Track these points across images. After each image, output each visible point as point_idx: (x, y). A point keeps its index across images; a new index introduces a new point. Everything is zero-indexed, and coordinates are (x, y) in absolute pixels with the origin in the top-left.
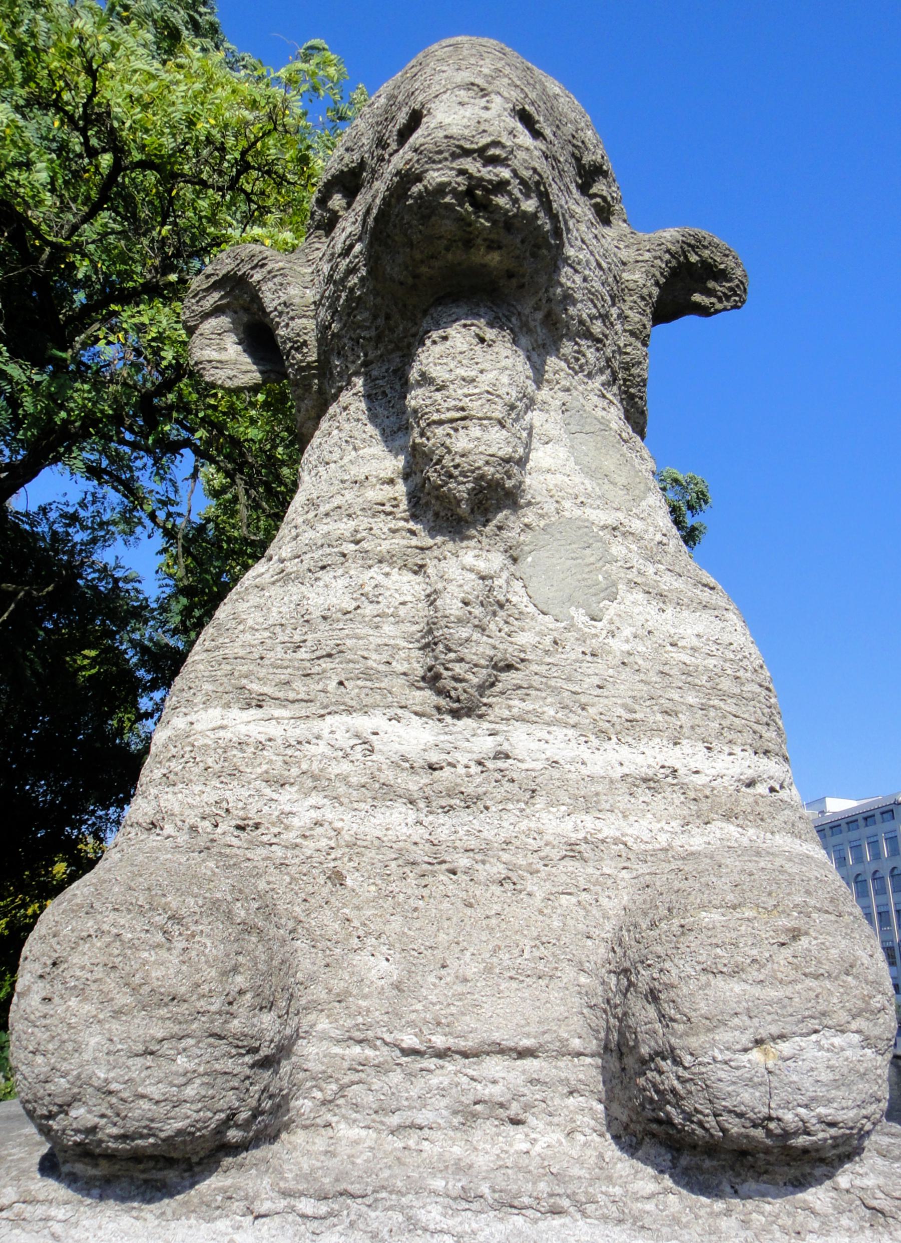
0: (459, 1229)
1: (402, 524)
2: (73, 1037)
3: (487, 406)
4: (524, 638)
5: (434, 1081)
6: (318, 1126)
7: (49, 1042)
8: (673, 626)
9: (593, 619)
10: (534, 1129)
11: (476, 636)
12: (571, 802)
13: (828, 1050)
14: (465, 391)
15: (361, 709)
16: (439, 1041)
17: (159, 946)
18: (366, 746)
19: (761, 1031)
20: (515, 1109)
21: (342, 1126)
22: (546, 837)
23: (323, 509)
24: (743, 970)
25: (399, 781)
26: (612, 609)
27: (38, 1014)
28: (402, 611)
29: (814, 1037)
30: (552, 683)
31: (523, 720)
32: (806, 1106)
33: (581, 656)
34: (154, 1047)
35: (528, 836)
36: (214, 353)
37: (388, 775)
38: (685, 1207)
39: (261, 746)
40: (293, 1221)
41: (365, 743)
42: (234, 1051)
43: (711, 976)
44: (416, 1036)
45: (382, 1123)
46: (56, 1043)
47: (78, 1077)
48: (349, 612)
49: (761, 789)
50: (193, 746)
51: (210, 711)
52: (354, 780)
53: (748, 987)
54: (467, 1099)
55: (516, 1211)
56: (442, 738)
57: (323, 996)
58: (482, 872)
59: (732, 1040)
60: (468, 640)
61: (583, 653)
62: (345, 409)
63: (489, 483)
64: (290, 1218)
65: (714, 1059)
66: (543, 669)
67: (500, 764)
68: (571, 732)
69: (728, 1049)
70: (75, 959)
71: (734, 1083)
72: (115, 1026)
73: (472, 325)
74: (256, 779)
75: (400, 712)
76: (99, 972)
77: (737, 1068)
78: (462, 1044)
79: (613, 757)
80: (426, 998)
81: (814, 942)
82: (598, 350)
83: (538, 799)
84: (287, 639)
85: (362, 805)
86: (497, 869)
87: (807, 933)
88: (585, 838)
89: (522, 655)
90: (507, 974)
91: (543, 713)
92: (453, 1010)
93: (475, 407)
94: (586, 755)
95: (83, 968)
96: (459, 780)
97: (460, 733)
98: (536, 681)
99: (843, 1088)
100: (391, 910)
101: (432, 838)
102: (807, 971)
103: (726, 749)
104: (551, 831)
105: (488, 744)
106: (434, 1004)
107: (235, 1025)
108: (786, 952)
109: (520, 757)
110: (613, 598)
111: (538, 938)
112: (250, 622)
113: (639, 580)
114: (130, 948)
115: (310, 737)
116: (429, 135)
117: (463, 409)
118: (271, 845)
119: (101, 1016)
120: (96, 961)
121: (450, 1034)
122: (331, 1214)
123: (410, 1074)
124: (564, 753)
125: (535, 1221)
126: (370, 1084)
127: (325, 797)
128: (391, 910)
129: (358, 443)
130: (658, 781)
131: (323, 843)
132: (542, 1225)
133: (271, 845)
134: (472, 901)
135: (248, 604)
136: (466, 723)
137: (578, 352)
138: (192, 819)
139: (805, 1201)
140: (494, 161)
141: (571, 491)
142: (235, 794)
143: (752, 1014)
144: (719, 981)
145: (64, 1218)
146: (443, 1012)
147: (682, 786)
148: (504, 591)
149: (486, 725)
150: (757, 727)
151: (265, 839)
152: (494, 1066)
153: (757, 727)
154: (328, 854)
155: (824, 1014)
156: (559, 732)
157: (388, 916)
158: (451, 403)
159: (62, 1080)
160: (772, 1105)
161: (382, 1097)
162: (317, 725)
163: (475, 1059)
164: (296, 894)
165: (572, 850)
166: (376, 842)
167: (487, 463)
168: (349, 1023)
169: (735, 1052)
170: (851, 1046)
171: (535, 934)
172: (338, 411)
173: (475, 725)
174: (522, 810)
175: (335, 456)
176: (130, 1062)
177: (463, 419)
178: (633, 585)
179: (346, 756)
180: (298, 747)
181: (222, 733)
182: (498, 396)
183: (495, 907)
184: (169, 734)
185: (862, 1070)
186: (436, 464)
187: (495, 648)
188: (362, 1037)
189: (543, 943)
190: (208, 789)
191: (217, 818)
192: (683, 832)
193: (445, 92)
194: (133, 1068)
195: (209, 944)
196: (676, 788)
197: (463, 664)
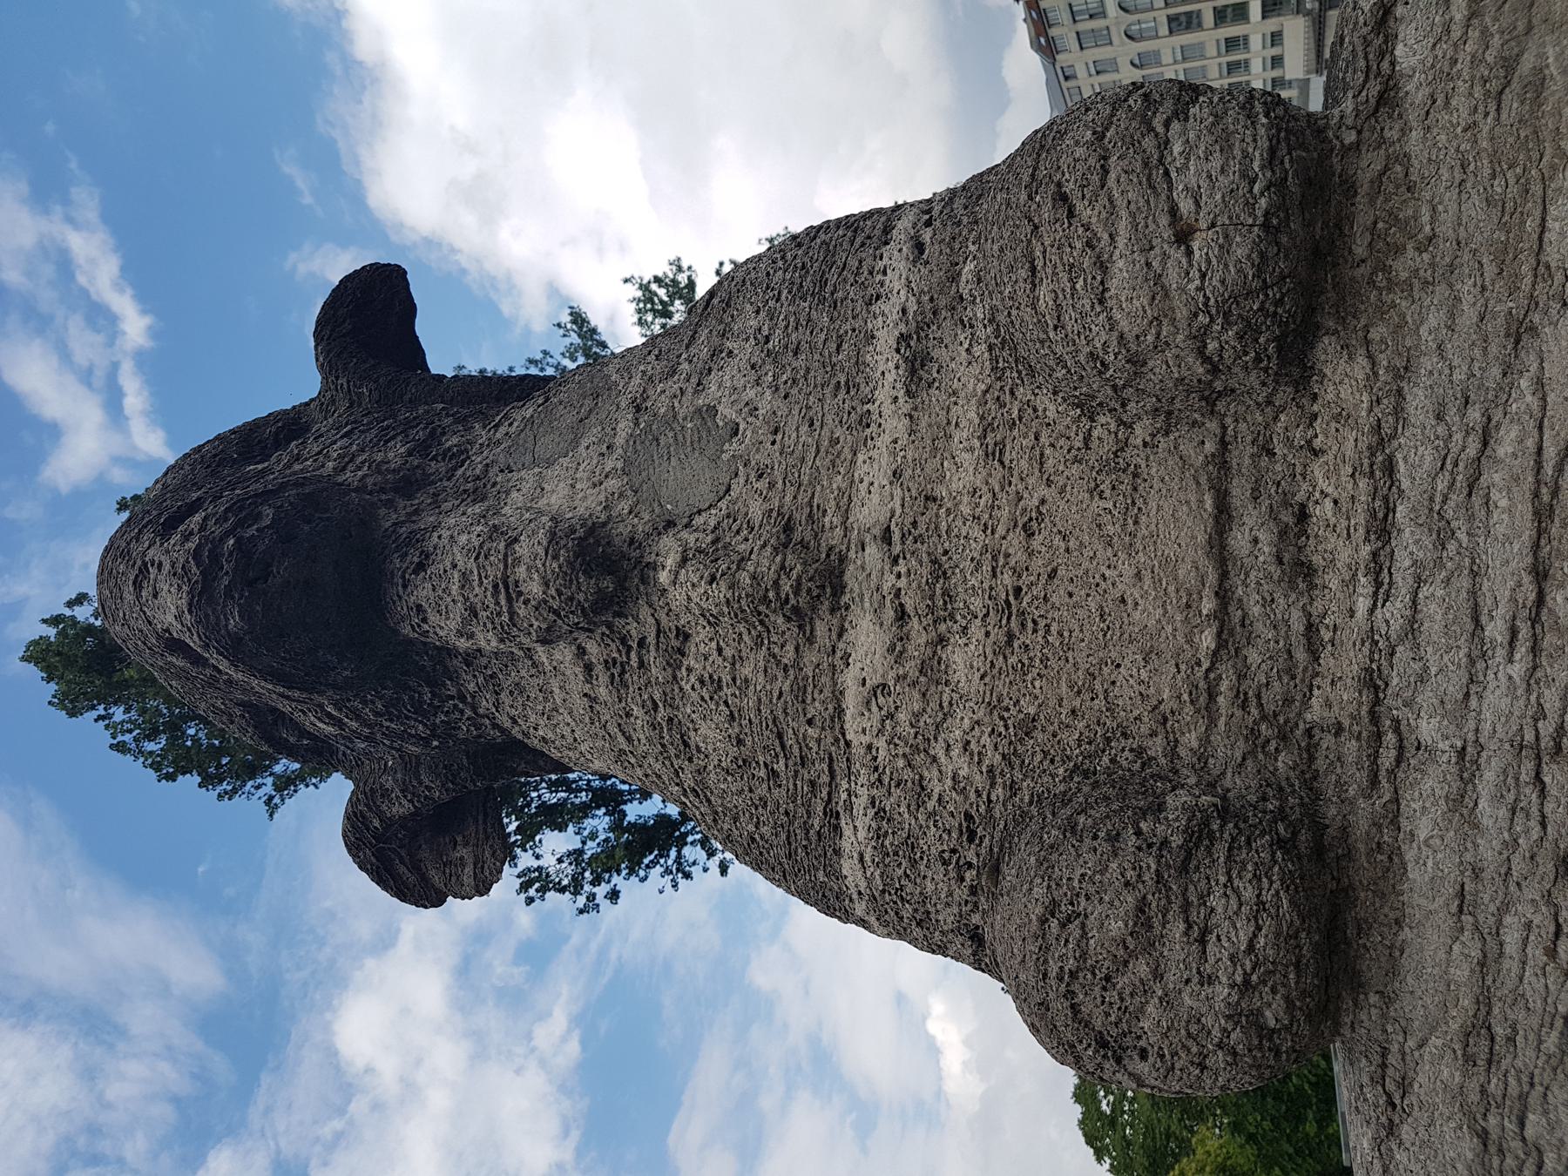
0: (1410, 580)
1: (633, 655)
2: (1183, 1024)
3: (492, 558)
4: (756, 510)
5: (1256, 610)
6: (1309, 744)
7: (1189, 1050)
8: (747, 340)
9: (736, 434)
10: (1311, 494)
11: (750, 567)
12: (939, 456)
13: (1188, 159)
14: (476, 583)
15: (839, 701)
16: (1208, 605)
17: (1083, 926)
18: (879, 692)
19: (1166, 236)
20: (1287, 517)
21: (1308, 717)
22: (978, 483)
23: (624, 746)
24: (1099, 257)
25: (916, 653)
26: (727, 412)
27: (1159, 1064)
28: (728, 652)
29: (1173, 175)
30: (805, 479)
31: (847, 511)
32: (1253, 182)
33: (776, 447)
34: (1195, 932)
35: (977, 505)
36: (466, 871)
37: (911, 668)
38: (1382, 319)
39: (880, 814)
40: (1405, 772)
41: (875, 695)
42: (1206, 842)
43: (1107, 295)
44: (1202, 632)
45: (1305, 670)
46: (1190, 1043)
47: (1228, 1017)
48: (731, 712)
49: (927, 235)
50: (883, 891)
51: (845, 872)
52: (916, 707)
53: (1117, 252)
54: (1275, 570)
55: (1391, 515)
56: (867, 605)
57: (1159, 740)
58: (1018, 557)
59: (1177, 269)
60: (753, 577)
61: (773, 443)
62: (515, 722)
63: (577, 556)
64: (1401, 775)
65: (1198, 289)
66: (790, 491)
67: (896, 537)
68: (861, 457)
69: (1188, 273)
70: (1098, 1023)
71: (1226, 266)
72: (1171, 978)
73: (403, 577)
74: (917, 819)
75: (839, 654)
76: (1112, 996)
77: (1209, 262)
78: (1212, 578)
79: (888, 409)
80: (1159, 621)
81: (1067, 176)
82: (444, 434)
83: (937, 493)
84: (765, 786)
85: (946, 698)
86: (1016, 539)
87: (1059, 185)
88: (979, 437)
89: (774, 514)
90: (1131, 527)
91: (839, 489)
92: (1171, 589)
93: (494, 571)
94: (887, 438)
95: (1107, 1015)
96: (914, 585)
97: (860, 584)
98: (803, 498)
99: (1232, 141)
100: (1062, 663)
101: (980, 615)
102: (1098, 184)
103: (879, 277)
104: (972, 478)
105: (873, 552)
106: (1166, 612)
107: (1177, 841)
108: (1079, 206)
109: (889, 515)
110: (712, 410)
111: (1091, 492)
112: (751, 828)
113: (694, 380)
114: (1085, 962)
115: (869, 757)
116: (189, 630)
117: (496, 586)
118: (990, 801)
119: (1160, 993)
120: (1099, 1000)
121: (1199, 593)
122: (1397, 731)
123: (1248, 639)
124: (884, 463)
125: (1401, 492)
126: (1259, 687)
127: (936, 739)
128: (1062, 663)
129: (549, 705)
130: (914, 356)
131: (986, 740)
132: (1405, 484)
133: (990, 801)
134: (1049, 569)
135: (734, 829)
136: (851, 576)
137: (444, 455)
138: (961, 893)
139: (1372, 182)
140: (215, 556)
141: (595, 461)
142: (932, 842)
143: (1147, 247)
144: (1113, 284)
145: (1402, 1034)
146: (1174, 601)
147: (919, 328)
148: (701, 535)
149: (852, 554)
150: (858, 241)
151: (982, 809)
152: (1239, 541)
153: (858, 241)
154: (1000, 734)
155: (1146, 164)
156: (861, 470)
157: (1068, 666)
158: (490, 600)
159: (1232, 1036)
160: (1250, 221)
161: (1275, 670)
162: (858, 751)
163: (1230, 564)
164: (1045, 771)
165: (993, 454)
166: (987, 680)
167: (555, 557)
168: (1189, 709)
169: (1191, 265)
170: (1184, 132)
171: (1087, 495)
172: (517, 729)
173: (851, 567)
174: (948, 511)
175: (567, 731)
176: (1212, 960)
177: (507, 588)
178: (701, 388)
179: (891, 716)
180: (881, 770)
181: (867, 858)
182: (481, 546)
183: (1056, 542)
184: (873, 918)
185: (1211, 119)
186: (559, 616)
187: (764, 546)
188: (1205, 695)
189: (1097, 486)
190: (930, 874)
191: (961, 863)
192: (972, 326)
193: (145, 613)
194: (1218, 956)
195: (1083, 871)
196: (922, 334)
197: (781, 582)
